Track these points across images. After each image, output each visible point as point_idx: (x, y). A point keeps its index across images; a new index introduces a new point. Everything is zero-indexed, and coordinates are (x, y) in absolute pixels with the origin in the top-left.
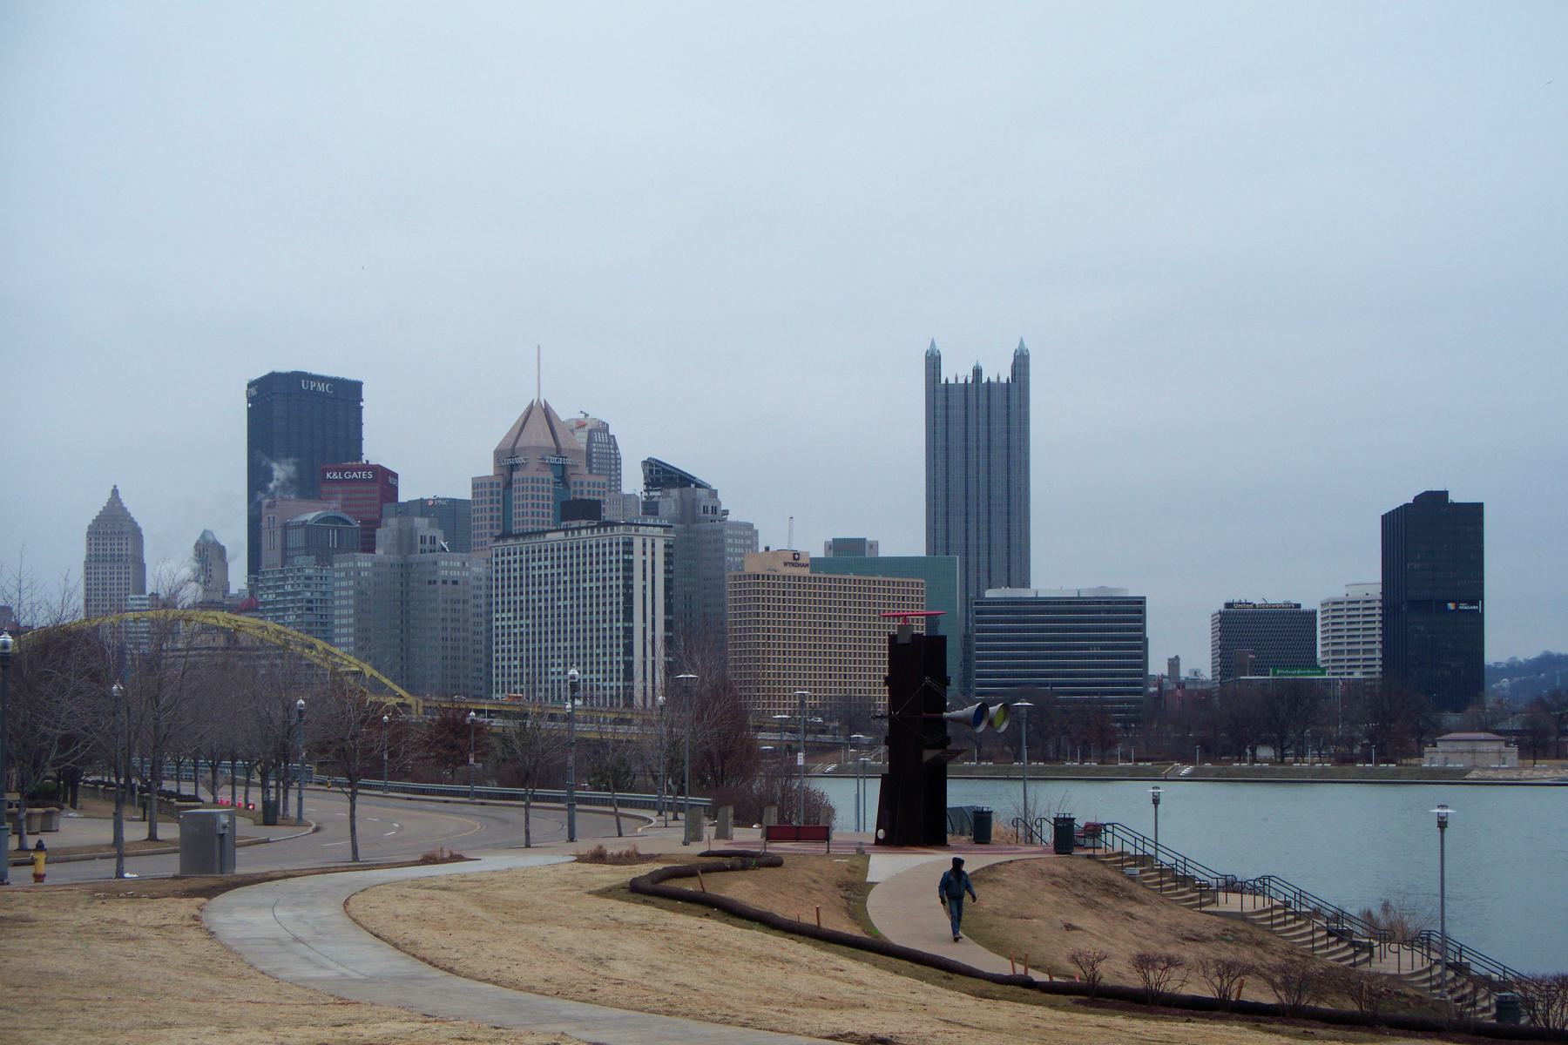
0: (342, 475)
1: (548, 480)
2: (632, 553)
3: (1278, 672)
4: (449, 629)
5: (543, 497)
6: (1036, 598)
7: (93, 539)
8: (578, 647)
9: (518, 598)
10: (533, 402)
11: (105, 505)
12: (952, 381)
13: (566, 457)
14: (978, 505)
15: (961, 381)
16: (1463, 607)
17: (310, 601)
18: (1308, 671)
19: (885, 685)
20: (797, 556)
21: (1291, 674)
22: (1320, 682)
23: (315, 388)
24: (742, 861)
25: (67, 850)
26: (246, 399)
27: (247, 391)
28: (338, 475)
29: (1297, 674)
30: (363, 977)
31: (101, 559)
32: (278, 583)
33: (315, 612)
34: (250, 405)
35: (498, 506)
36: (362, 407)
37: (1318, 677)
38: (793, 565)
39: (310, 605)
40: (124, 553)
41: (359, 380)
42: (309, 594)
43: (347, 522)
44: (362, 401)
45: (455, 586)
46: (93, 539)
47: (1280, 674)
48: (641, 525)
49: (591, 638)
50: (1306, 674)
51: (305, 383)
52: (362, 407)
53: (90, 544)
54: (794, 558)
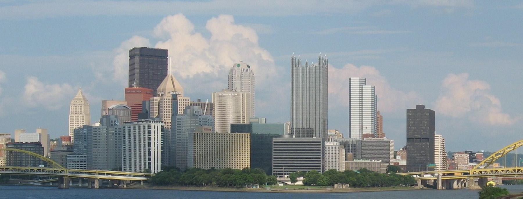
1: (170, 99)
2: (151, 129)
5: (168, 104)
7: (72, 106)
8: (199, 149)
9: (129, 140)
13: (177, 92)
14: (306, 116)
19: (211, 167)
22: (359, 163)
24: (266, 189)
30: (487, 167)
31: (77, 113)
35: (155, 106)
36: (167, 59)
39: (85, 137)
40: (82, 111)
44: (168, 56)
45: (119, 133)
46: (72, 106)
48: (141, 121)
49: (208, 147)
52: (167, 59)
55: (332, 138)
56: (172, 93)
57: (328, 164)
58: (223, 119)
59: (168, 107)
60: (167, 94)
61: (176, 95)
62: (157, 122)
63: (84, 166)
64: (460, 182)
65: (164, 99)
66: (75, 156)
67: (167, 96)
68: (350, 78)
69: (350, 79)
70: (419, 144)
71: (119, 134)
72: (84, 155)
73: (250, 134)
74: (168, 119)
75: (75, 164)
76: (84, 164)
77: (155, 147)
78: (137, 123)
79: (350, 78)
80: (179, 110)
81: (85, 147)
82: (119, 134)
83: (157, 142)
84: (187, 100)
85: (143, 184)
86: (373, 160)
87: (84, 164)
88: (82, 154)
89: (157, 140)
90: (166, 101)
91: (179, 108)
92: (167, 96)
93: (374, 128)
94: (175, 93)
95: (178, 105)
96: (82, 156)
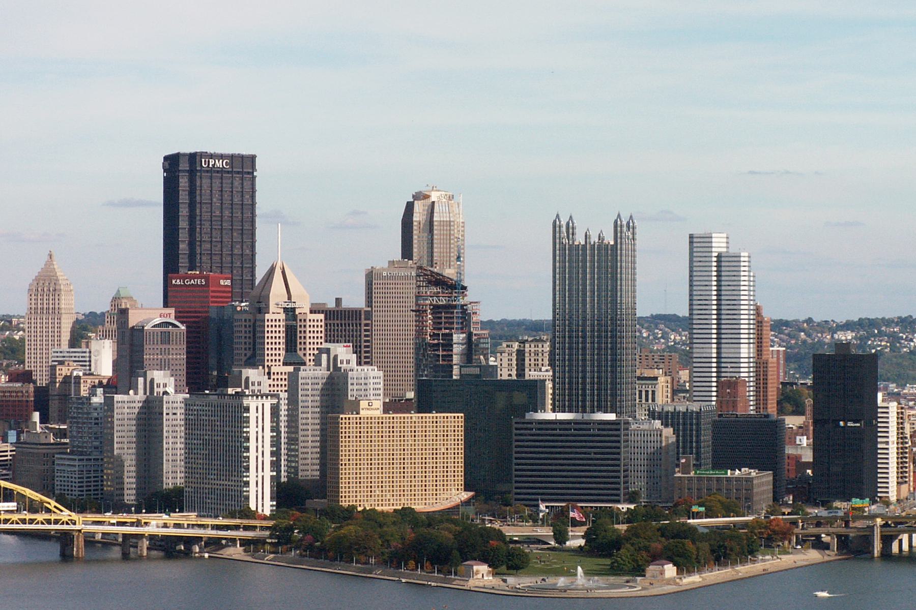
0: (184, 282)
3: (698, 472)
4: (170, 443)
6: (556, 420)
10: (273, 264)
11: (43, 266)
12: (594, 239)
15: (594, 239)
16: (850, 424)
17: (97, 419)
18: (717, 472)
20: (370, 404)
21: (706, 474)
23: (214, 165)
25: (757, 376)
26: (163, 170)
27: (163, 163)
28: (180, 281)
29: (710, 474)
32: (79, 406)
33: (100, 425)
34: (165, 175)
37: (722, 476)
38: (368, 409)
41: (253, 154)
42: (96, 414)
43: (177, 327)
44: (256, 171)
47: (699, 474)
50: (716, 474)
51: (205, 161)
53: (31, 300)
54: (369, 405)
55: (647, 389)
56: (285, 305)
57: (637, 471)
58: (394, 304)
59: (276, 343)
60: (272, 308)
61: (294, 309)
62: (262, 397)
63: (94, 481)
64: (897, 540)
65: (266, 320)
66: (76, 460)
67: (273, 313)
68: (690, 235)
69: (690, 237)
70: (875, 343)
71: (175, 414)
72: (94, 457)
73: (462, 415)
74: (276, 365)
75: (73, 476)
76: (94, 477)
77: (257, 451)
78: (218, 397)
79: (690, 235)
80: (300, 343)
81: (95, 438)
82: (175, 414)
83: (263, 447)
84: (314, 321)
85: (168, 370)
86: (729, 471)
87: (94, 477)
88: (89, 455)
89: (263, 442)
90: (270, 323)
91: (300, 337)
92: (273, 313)
93: (749, 353)
94: (290, 306)
95: (298, 338)
96: (90, 459)
